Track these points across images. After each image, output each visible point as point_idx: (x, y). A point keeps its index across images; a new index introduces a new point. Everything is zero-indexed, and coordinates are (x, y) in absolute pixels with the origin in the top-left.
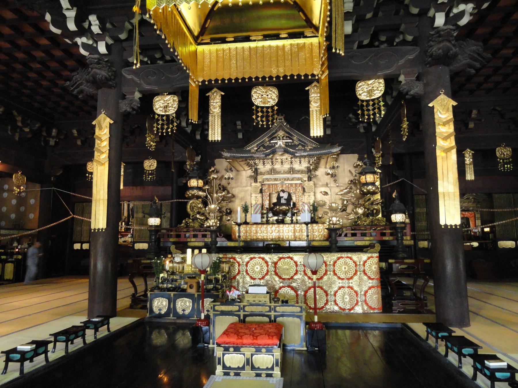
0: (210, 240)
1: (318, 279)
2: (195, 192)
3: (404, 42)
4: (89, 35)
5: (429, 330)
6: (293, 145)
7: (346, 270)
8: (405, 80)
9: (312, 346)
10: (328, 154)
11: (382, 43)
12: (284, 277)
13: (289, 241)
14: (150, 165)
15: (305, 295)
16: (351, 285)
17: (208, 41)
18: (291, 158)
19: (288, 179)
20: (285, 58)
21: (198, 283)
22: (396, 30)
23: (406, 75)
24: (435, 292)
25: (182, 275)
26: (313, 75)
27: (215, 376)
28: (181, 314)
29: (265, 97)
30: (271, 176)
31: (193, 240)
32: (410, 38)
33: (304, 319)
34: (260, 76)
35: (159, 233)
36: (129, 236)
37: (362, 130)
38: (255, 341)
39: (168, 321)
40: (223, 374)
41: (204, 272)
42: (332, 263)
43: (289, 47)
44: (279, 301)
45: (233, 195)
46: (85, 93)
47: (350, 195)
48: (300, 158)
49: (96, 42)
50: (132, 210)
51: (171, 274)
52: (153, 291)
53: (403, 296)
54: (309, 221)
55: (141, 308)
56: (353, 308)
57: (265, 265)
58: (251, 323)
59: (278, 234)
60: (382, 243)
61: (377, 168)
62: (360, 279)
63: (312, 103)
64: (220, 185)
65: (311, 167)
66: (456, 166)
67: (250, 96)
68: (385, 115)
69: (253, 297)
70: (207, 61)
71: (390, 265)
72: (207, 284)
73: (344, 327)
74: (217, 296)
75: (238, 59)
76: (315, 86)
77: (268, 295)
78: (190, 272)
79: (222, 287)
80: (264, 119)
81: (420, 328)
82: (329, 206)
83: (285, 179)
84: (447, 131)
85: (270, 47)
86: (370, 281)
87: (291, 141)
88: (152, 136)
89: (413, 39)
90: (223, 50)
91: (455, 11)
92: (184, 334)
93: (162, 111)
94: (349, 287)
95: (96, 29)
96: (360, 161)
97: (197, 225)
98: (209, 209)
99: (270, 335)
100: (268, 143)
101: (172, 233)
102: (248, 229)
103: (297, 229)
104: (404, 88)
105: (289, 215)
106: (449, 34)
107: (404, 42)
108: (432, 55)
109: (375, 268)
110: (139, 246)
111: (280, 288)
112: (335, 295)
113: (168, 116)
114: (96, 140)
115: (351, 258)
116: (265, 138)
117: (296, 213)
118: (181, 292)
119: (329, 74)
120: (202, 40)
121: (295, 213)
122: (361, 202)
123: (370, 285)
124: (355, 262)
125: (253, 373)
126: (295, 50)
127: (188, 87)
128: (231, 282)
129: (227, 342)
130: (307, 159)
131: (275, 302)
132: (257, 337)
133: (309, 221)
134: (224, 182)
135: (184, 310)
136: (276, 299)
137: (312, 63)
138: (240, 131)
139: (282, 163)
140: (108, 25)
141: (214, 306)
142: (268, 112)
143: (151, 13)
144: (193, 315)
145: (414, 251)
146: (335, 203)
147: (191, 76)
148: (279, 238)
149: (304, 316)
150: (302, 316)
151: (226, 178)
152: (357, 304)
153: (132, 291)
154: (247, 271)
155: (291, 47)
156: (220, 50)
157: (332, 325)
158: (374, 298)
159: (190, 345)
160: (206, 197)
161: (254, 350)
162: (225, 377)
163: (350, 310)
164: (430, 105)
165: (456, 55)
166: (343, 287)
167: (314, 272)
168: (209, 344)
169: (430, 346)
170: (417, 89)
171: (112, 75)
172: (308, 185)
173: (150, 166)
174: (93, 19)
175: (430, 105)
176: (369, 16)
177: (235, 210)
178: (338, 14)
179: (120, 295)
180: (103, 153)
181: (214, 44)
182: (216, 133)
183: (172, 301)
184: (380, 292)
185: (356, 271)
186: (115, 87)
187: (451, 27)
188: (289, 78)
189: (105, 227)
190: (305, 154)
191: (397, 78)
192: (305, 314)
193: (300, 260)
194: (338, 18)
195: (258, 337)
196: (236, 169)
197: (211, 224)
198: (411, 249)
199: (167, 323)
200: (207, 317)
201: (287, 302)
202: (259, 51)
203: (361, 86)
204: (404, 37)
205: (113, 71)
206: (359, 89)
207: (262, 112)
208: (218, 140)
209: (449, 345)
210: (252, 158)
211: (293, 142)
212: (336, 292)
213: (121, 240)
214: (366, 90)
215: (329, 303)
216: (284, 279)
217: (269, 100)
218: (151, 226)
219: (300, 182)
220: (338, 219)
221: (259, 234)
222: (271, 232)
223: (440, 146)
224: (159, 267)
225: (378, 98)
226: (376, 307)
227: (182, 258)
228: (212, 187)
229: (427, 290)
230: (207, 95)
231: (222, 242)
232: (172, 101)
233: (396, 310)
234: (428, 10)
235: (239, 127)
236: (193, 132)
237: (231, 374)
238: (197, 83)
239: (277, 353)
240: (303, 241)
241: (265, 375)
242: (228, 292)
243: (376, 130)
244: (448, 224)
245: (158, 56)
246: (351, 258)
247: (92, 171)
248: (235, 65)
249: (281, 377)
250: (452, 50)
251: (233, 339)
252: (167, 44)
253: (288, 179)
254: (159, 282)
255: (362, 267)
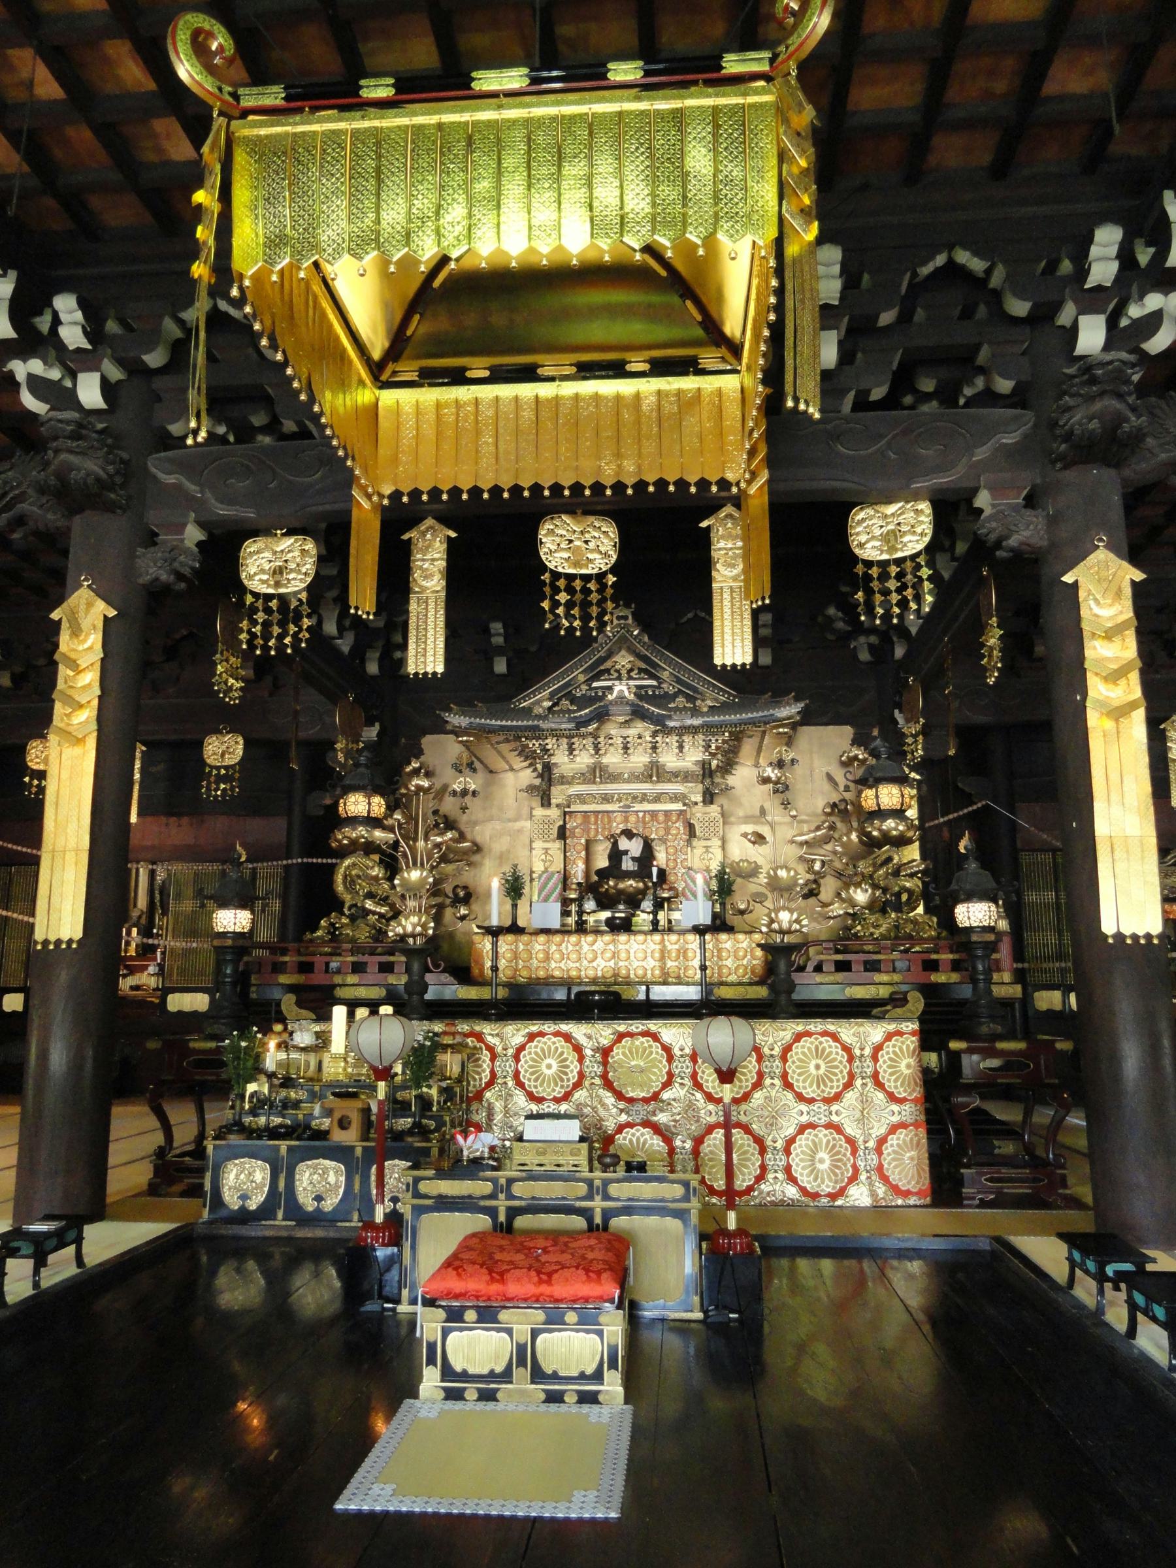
0: (404, 979)
1: (736, 1101)
2: (361, 831)
3: (989, 397)
4: (52, 353)
5: (1077, 1256)
6: (660, 696)
7: (822, 1071)
8: (993, 506)
9: (722, 1307)
10: (766, 723)
11: (927, 397)
12: (631, 1095)
13: (648, 985)
14: (224, 750)
15: (696, 1152)
16: (835, 1118)
17: (413, 376)
18: (655, 734)
19: (644, 798)
20: (639, 430)
21: (367, 1111)
22: (963, 362)
23: (992, 489)
24: (1090, 1146)
25: (318, 1087)
26: (724, 484)
27: (417, 1403)
28: (310, 1209)
29: (578, 547)
30: (594, 787)
31: (352, 979)
32: (1004, 385)
33: (694, 1218)
34: (567, 482)
35: (246, 959)
36: (152, 969)
37: (864, 656)
38: (544, 1289)
39: (269, 1233)
40: (442, 1394)
41: (384, 1073)
42: (777, 1051)
43: (653, 399)
44: (615, 1164)
45: (475, 844)
46: (31, 523)
47: (829, 847)
48: (680, 735)
49: (73, 376)
50: (164, 890)
51: (282, 1085)
52: (224, 1139)
53: (992, 1154)
54: (708, 922)
55: (184, 1194)
56: (842, 1192)
57: (572, 1056)
58: (532, 1234)
59: (612, 963)
60: (930, 991)
61: (908, 766)
62: (864, 1100)
63: (718, 566)
64: (436, 812)
65: (714, 763)
66: (1146, 759)
67: (533, 544)
68: (934, 606)
69: (539, 1153)
70: (408, 433)
71: (955, 1057)
72: (395, 1117)
73: (817, 1250)
74: (426, 1152)
75: (501, 431)
76: (729, 516)
77: (585, 1145)
78: (341, 1077)
79: (441, 1124)
80: (575, 612)
81: (1048, 1253)
82: (769, 876)
83: (635, 798)
84: (1119, 654)
85: (596, 397)
86: (895, 1107)
87: (654, 683)
88: (232, 660)
89: (1014, 389)
90: (458, 404)
91: (1135, 311)
92: (317, 1275)
93: (263, 582)
94: (829, 1126)
95: (73, 335)
96: (859, 746)
97: (363, 934)
98: (405, 883)
99: (589, 1270)
100: (584, 687)
101: (287, 959)
102: (521, 947)
103: (669, 947)
104: (989, 528)
105: (647, 905)
106: (1119, 375)
107: (989, 397)
108: (1071, 433)
109: (908, 1066)
110: (180, 1002)
111: (620, 1128)
112: (787, 1151)
113: (282, 598)
114: (61, 667)
115: (835, 1037)
116: (576, 674)
117: (668, 899)
118: (312, 1141)
119: (770, 482)
120: (394, 373)
121: (664, 899)
122: (863, 866)
123: (895, 1119)
124: (847, 1049)
125: (538, 1391)
126: (670, 408)
127: (349, 513)
128: (468, 1111)
129: (458, 1291)
130: (700, 738)
131: (605, 1168)
132: (550, 1275)
133: (708, 922)
134: (449, 806)
135: (319, 1198)
136: (608, 1160)
137: (722, 448)
138: (500, 651)
139: (626, 748)
140: (112, 326)
141: (417, 1180)
142: (586, 591)
143: (247, 283)
144: (350, 1213)
145: (1020, 1018)
146: (788, 869)
147: (358, 478)
148: (616, 975)
149: (694, 1212)
150: (688, 1211)
151: (454, 793)
152: (853, 1179)
153: (159, 1139)
154: (517, 1074)
155: (659, 401)
156: (447, 404)
157: (782, 1243)
158: (908, 1161)
159: (336, 1306)
160: (396, 845)
161: (540, 1316)
162: (450, 1404)
163: (833, 1196)
164: (1068, 578)
165: (1138, 437)
166: (812, 1126)
167: (726, 1076)
168: (398, 1301)
169: (1081, 1306)
170: (1028, 532)
171: (118, 472)
172: (702, 814)
173: (223, 754)
174: (66, 305)
175: (1068, 578)
176: (886, 318)
177: (480, 890)
178: (803, 301)
179: (116, 1154)
180: (81, 706)
181: (431, 385)
182: (430, 652)
183: (282, 1171)
184: (925, 1141)
185: (852, 1076)
186: (124, 511)
187: (1124, 355)
188: (651, 489)
189: (78, 934)
190: (697, 722)
191: (969, 501)
192: (699, 1205)
193: (682, 1042)
194: (801, 318)
195: (555, 1276)
196: (486, 766)
197: (409, 929)
198: (1013, 1009)
199: (265, 1238)
200: (394, 1218)
201: (642, 1167)
202: (563, 411)
203: (863, 520)
204: (988, 381)
205: (122, 461)
206: (858, 529)
207: (570, 590)
208: (435, 673)
209: (1140, 1299)
210: (536, 732)
211: (659, 687)
212: (790, 1141)
213: (125, 984)
214: (877, 532)
215: (770, 1176)
216: (631, 1101)
217: (591, 556)
218: (223, 935)
219: (678, 806)
220: (795, 916)
221: (553, 965)
222: (591, 958)
223: (1098, 701)
224: (246, 1060)
225: (913, 557)
226: (912, 1186)
227: (318, 1035)
228: (412, 819)
229: (1064, 1138)
230: (405, 537)
231: (442, 987)
232: (297, 553)
233: (974, 1198)
234: (1057, 307)
235: (498, 640)
236: (359, 652)
237: (467, 1395)
238: (375, 498)
239: (614, 1326)
240: (688, 984)
241: (575, 1398)
242: (459, 1138)
243: (906, 656)
244: (1127, 932)
245: (259, 420)
246: (835, 1037)
247: (42, 767)
248: (492, 449)
249: (626, 1403)
250: (1127, 420)
251: (477, 1283)
252: (290, 380)
253: (644, 798)
254: (243, 1108)
255: (869, 1062)
